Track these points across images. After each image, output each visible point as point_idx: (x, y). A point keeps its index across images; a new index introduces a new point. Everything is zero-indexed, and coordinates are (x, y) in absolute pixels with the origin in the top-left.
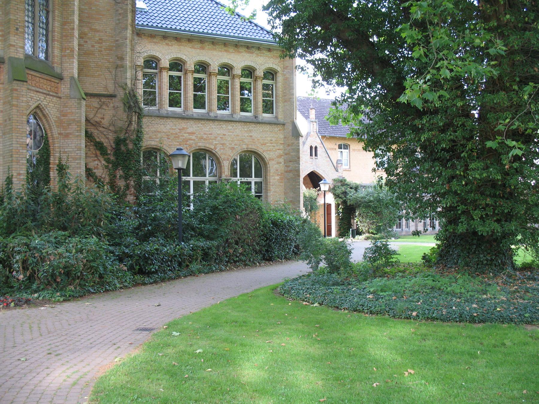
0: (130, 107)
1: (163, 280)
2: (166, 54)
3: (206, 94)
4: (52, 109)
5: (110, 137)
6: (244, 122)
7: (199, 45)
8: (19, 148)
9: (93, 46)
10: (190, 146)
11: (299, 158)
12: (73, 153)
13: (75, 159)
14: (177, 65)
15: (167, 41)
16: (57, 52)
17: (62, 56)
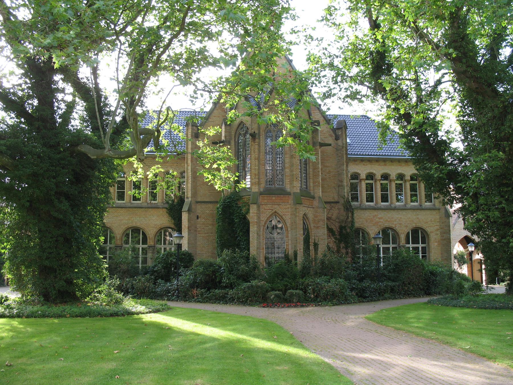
0: (347, 209)
1: (372, 301)
2: (363, 170)
3: (389, 193)
4: (310, 216)
5: (337, 226)
6: (413, 209)
7: (383, 163)
9: (326, 175)
10: (380, 226)
11: (450, 231)
12: (321, 236)
13: (322, 240)
14: (370, 176)
15: (364, 163)
16: (311, 184)
17: (314, 186)
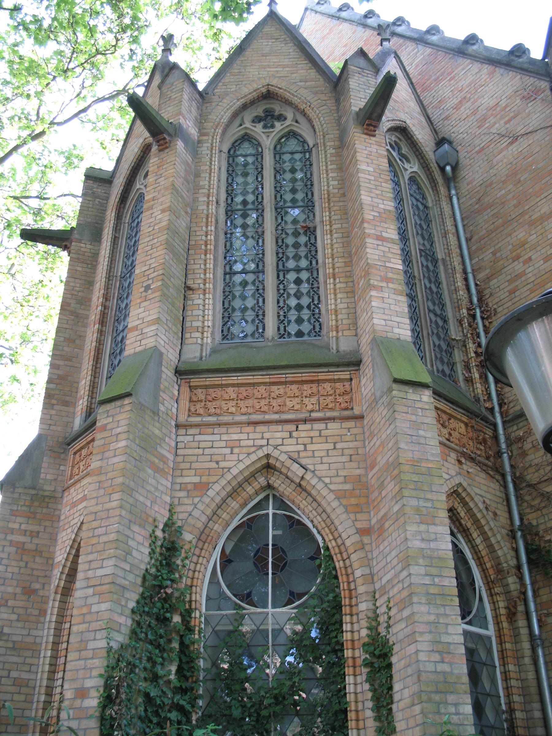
8: (90, 601)
